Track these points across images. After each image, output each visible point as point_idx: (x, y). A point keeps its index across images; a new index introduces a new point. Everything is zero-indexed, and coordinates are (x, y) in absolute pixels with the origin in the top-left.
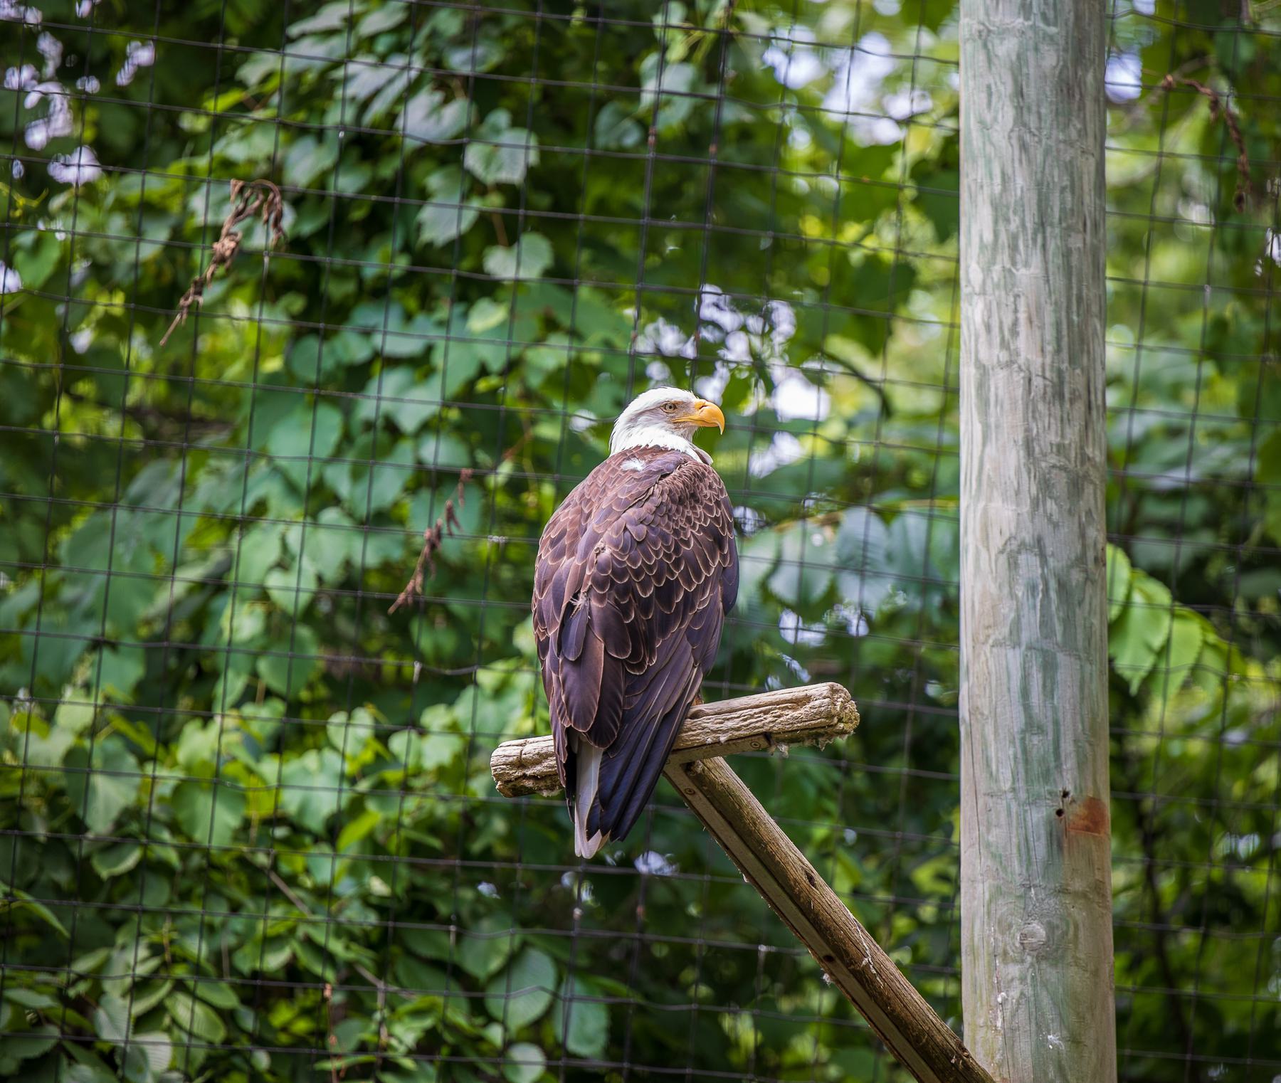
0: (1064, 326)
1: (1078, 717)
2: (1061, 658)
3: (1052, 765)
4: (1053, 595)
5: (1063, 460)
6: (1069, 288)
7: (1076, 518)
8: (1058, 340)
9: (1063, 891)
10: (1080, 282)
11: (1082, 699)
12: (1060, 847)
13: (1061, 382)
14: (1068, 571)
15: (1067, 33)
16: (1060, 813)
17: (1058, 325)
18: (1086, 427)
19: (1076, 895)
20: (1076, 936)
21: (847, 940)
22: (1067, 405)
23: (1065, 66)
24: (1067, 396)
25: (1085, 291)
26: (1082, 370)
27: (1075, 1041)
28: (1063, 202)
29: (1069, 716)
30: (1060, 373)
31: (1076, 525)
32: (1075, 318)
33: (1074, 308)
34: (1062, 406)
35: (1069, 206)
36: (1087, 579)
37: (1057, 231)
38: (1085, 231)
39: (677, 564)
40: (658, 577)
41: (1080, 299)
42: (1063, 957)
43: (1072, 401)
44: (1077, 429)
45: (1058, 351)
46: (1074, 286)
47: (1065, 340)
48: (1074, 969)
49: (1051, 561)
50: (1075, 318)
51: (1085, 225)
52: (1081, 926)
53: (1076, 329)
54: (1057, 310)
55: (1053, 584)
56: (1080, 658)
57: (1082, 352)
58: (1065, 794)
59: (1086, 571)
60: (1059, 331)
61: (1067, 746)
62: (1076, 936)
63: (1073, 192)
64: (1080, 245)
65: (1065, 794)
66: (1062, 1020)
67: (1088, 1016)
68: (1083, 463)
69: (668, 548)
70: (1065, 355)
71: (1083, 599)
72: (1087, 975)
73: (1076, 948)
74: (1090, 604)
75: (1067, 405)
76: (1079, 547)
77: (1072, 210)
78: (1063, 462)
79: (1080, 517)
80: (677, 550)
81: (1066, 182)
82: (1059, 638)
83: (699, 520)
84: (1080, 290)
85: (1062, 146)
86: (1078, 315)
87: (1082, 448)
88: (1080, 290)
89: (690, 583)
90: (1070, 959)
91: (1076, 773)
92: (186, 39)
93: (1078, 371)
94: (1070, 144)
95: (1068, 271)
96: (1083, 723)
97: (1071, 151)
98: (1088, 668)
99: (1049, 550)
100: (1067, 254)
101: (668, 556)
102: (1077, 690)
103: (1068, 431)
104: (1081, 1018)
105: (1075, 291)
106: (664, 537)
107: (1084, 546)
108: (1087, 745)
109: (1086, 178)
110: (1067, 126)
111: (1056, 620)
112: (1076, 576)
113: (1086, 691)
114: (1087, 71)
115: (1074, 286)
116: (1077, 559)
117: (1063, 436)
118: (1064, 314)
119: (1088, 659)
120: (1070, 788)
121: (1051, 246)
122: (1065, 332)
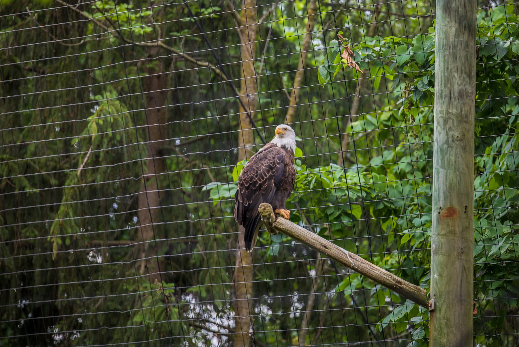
0: (443, 77)
1: (445, 186)
2: (441, 170)
6: (445, 66)
7: (445, 130)
9: (439, 235)
11: (446, 180)
12: (439, 222)
13: (442, 93)
14: (285, 168)
16: (439, 213)
17: (441, 77)
18: (449, 104)
20: (442, 247)
21: (343, 261)
22: (443, 99)
24: (443, 97)
25: (449, 66)
26: (448, 88)
28: (443, 42)
29: (442, 186)
30: (442, 91)
32: (446, 74)
33: (446, 71)
34: (442, 99)
35: (445, 43)
36: (448, 147)
38: (450, 49)
39: (256, 176)
41: (448, 68)
42: (438, 253)
43: (444, 98)
44: (446, 105)
45: (441, 84)
47: (443, 82)
48: (441, 256)
49: (439, 143)
50: (446, 74)
51: (450, 47)
52: (444, 244)
53: (446, 77)
54: (441, 73)
55: (439, 150)
57: (448, 83)
58: (440, 208)
59: (448, 144)
60: (441, 79)
61: (441, 194)
62: (442, 247)
64: (448, 53)
65: (440, 208)
67: (445, 268)
68: (447, 114)
70: (443, 85)
71: (447, 152)
72: (445, 257)
73: (442, 249)
74: (450, 153)
75: (443, 99)
76: (446, 138)
77: (446, 44)
78: (442, 115)
80: (257, 172)
81: (444, 37)
84: (448, 66)
85: (443, 27)
87: (447, 110)
88: (448, 66)
89: (260, 181)
90: (440, 253)
91: (443, 201)
93: (446, 89)
94: (446, 26)
96: (446, 187)
97: (446, 28)
98: (449, 171)
99: (438, 140)
100: (444, 57)
101: (254, 175)
102: (444, 178)
103: (443, 106)
104: (442, 269)
105: (446, 67)
106: (254, 170)
107: (448, 138)
108: (448, 193)
109: (451, 34)
110: (445, 21)
112: (445, 146)
113: (448, 178)
117: (442, 108)
120: (441, 206)
122: (443, 79)
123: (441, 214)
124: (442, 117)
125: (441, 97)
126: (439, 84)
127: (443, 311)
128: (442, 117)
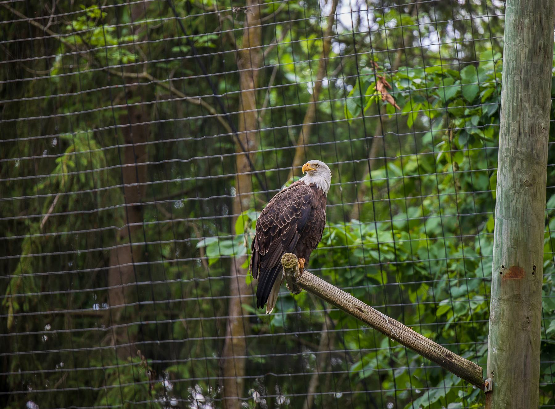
1: (509, 240)
2: (505, 221)
3: (500, 257)
4: (503, 200)
5: (508, 153)
6: (514, 94)
8: (509, 113)
10: (518, 92)
11: (511, 234)
12: (500, 285)
15: (517, 7)
16: (501, 273)
17: (509, 107)
19: (505, 300)
23: (516, 19)
24: (511, 131)
25: (520, 94)
26: (517, 122)
27: (500, 349)
30: (509, 124)
31: (512, 175)
37: (511, 76)
38: (521, 74)
39: (277, 219)
40: (270, 224)
41: (517, 97)
45: (509, 116)
46: (515, 93)
47: (511, 114)
54: (509, 103)
55: (503, 196)
56: (511, 220)
57: (517, 115)
58: (503, 267)
60: (509, 110)
62: (503, 314)
63: (516, 62)
65: (503, 267)
66: (497, 343)
68: (515, 153)
69: (274, 215)
70: (511, 118)
73: (503, 318)
77: (516, 68)
79: (513, 172)
82: (504, 214)
83: (289, 204)
84: (517, 94)
86: (516, 103)
88: (517, 94)
89: (281, 225)
90: (500, 322)
92: (181, 80)
95: (513, 88)
98: (515, 222)
99: (503, 185)
100: (514, 82)
101: (274, 217)
102: (509, 231)
109: (522, 56)
110: (515, 39)
111: (503, 208)
114: (525, 19)
115: (515, 93)
116: (511, 187)
118: (511, 104)
119: (514, 220)
120: (504, 264)
121: (509, 82)
122: (511, 110)
123: (504, 274)
124: (508, 156)
125: (508, 132)
126: (506, 116)
127: (502, 393)
128: (508, 156)
